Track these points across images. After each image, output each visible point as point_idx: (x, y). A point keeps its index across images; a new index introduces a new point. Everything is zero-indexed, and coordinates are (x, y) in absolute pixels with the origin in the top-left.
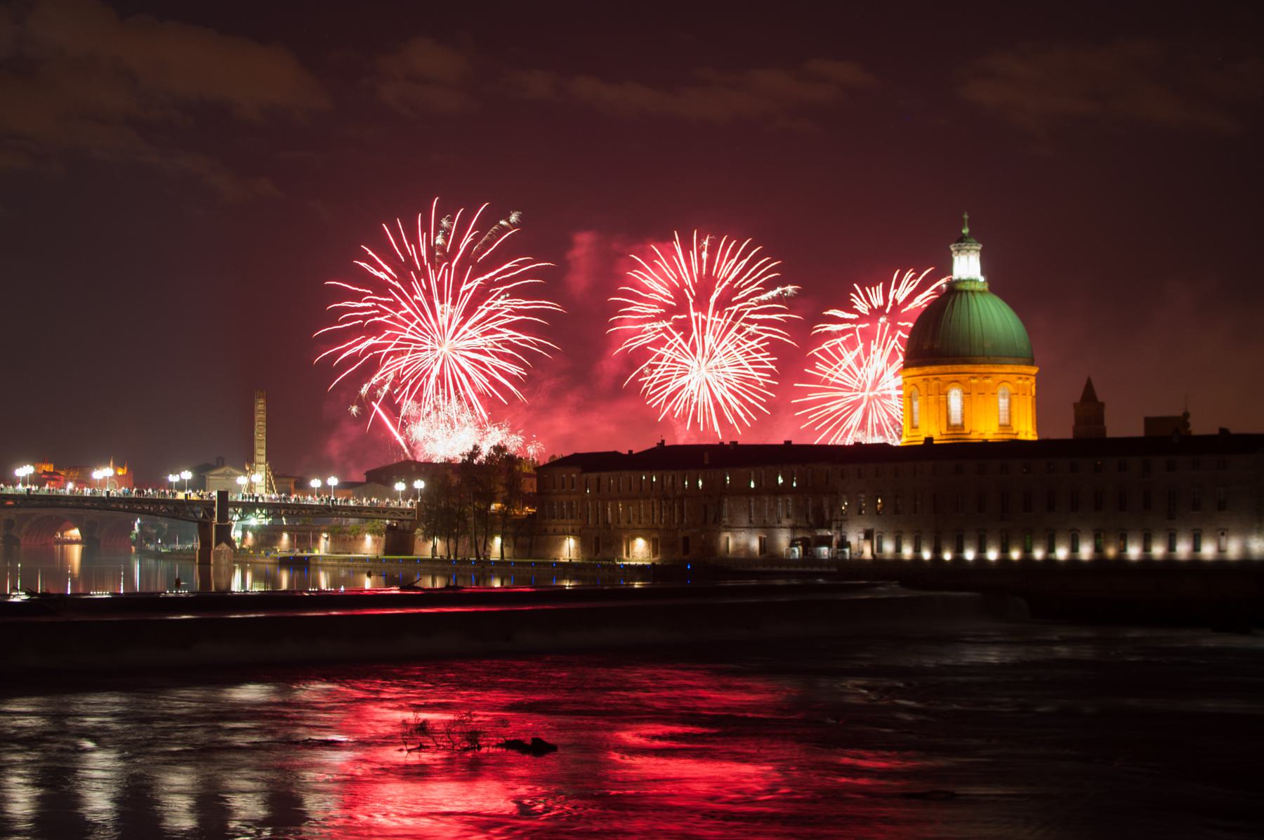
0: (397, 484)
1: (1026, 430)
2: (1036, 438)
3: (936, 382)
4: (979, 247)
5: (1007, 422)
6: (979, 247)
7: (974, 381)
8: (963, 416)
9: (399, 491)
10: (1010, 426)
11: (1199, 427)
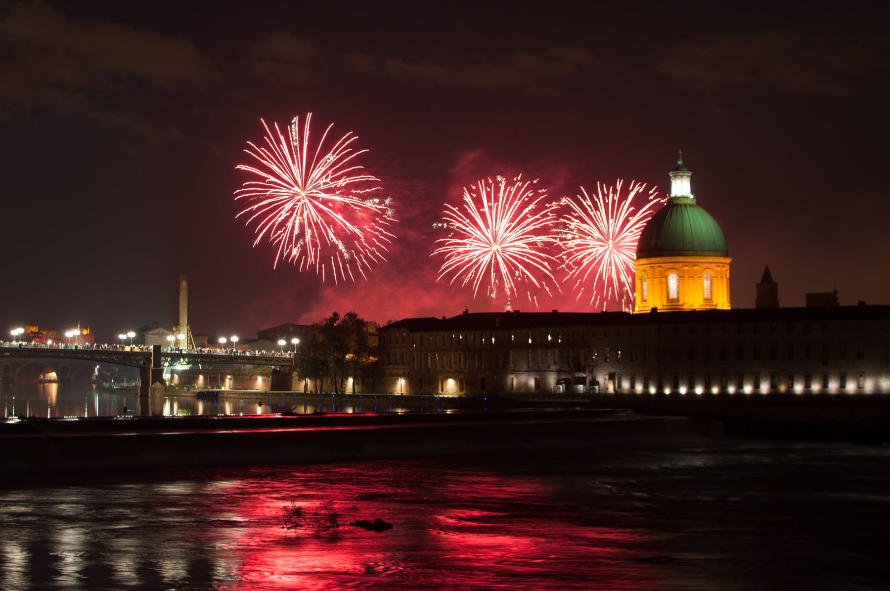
1: (723, 303)
2: (729, 308)
5: (709, 297)
7: (719, 269)
8: (678, 293)
10: (711, 299)
11: (844, 301)
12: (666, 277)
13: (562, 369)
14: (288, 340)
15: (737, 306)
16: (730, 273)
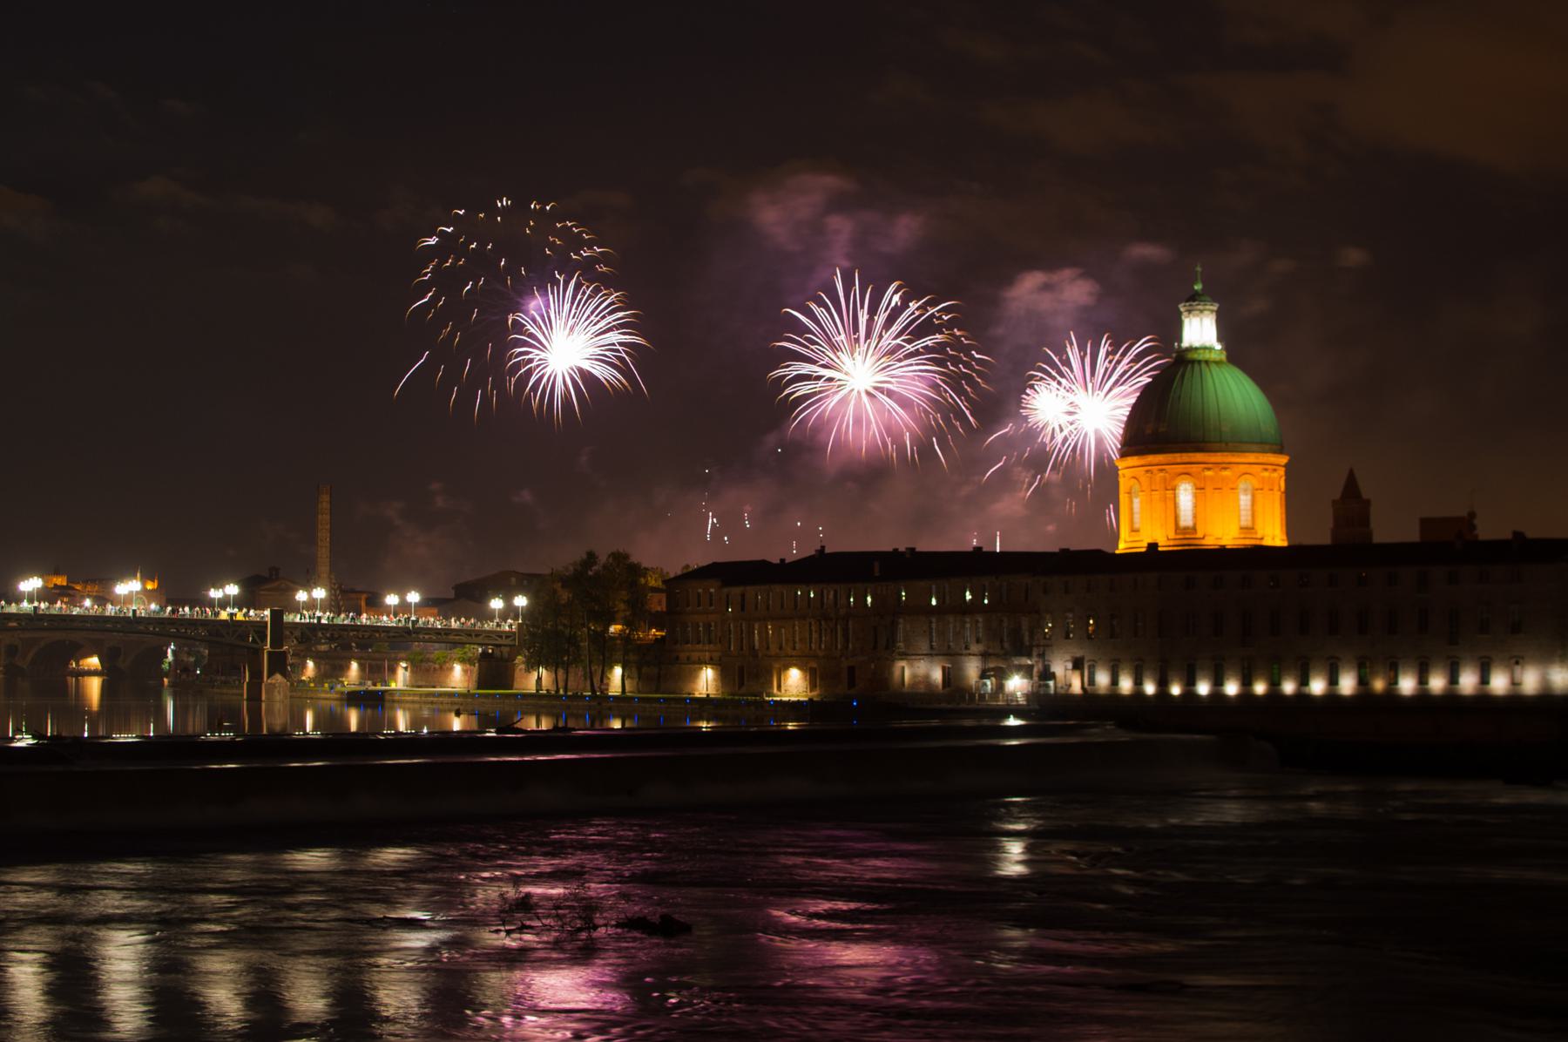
1: (1274, 534)
2: (1285, 544)
3: (1162, 474)
4: (1215, 307)
5: (1249, 524)
6: (1215, 307)
8: (1195, 516)
9: (495, 610)
10: (1253, 528)
12: (1174, 489)
13: (991, 651)
14: (508, 599)
16: (1286, 480)
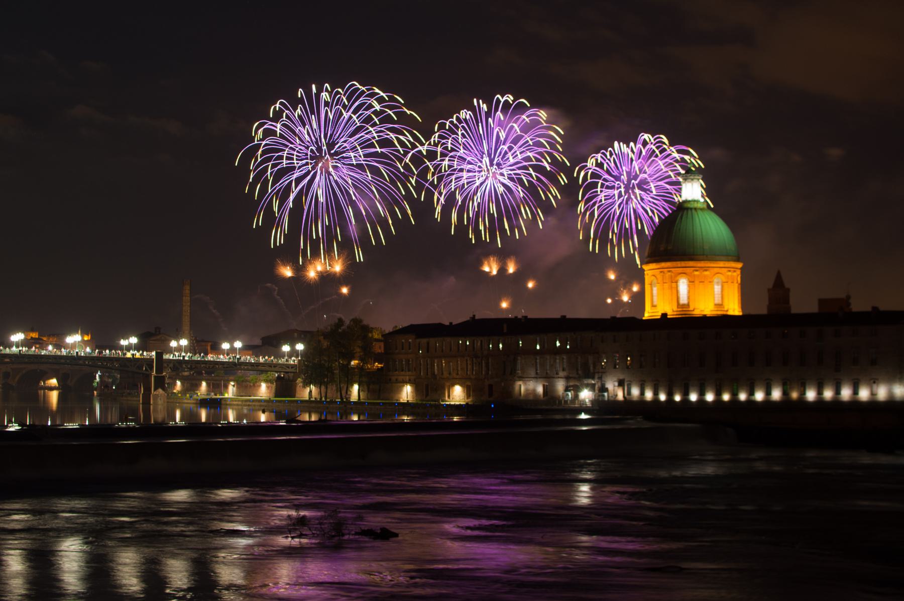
0: (284, 346)
1: (734, 308)
2: (741, 314)
5: (720, 302)
7: (697, 273)
8: (689, 298)
10: (722, 305)
12: (677, 282)
15: (747, 312)
